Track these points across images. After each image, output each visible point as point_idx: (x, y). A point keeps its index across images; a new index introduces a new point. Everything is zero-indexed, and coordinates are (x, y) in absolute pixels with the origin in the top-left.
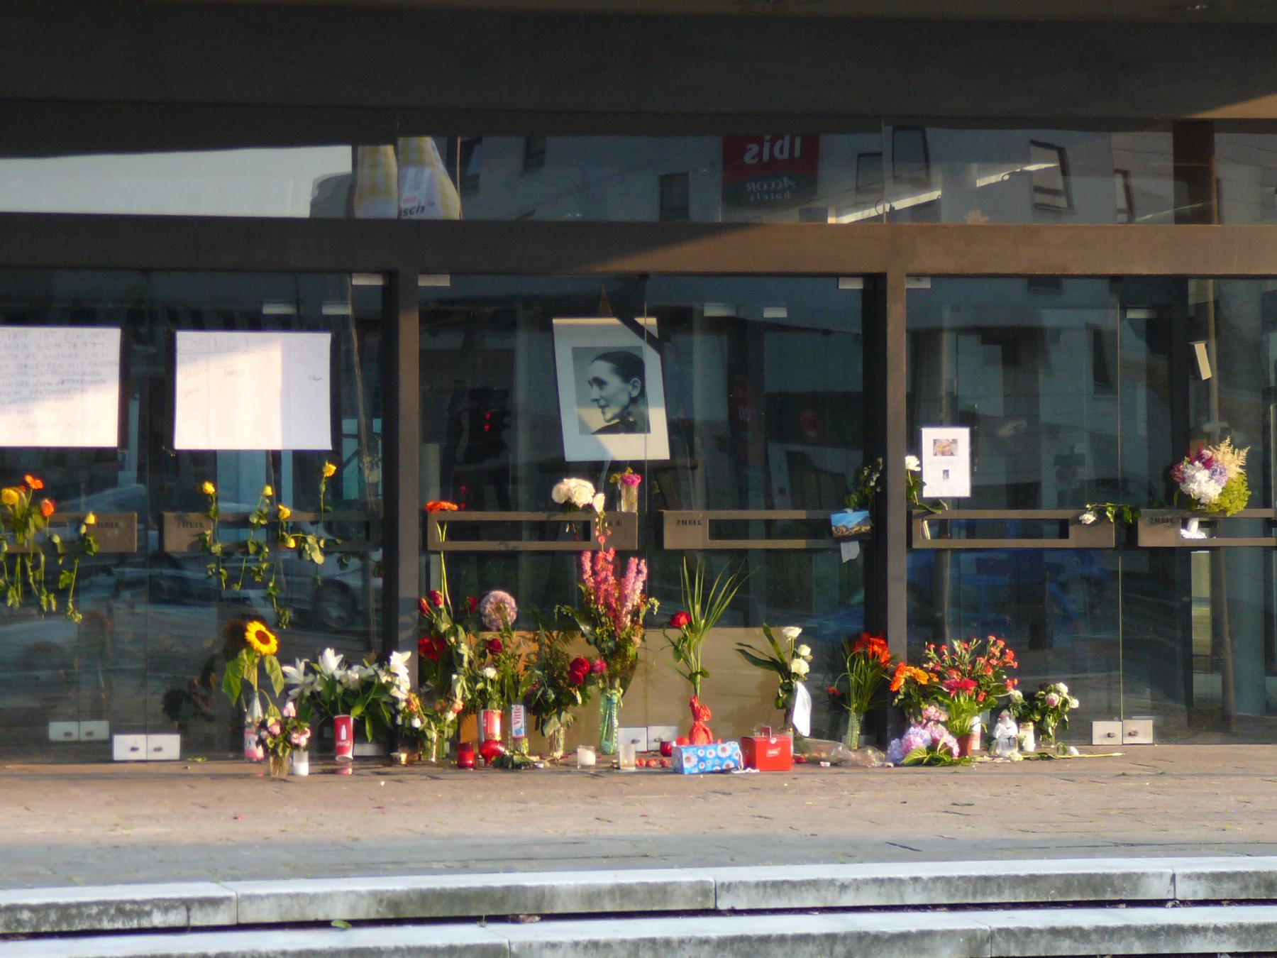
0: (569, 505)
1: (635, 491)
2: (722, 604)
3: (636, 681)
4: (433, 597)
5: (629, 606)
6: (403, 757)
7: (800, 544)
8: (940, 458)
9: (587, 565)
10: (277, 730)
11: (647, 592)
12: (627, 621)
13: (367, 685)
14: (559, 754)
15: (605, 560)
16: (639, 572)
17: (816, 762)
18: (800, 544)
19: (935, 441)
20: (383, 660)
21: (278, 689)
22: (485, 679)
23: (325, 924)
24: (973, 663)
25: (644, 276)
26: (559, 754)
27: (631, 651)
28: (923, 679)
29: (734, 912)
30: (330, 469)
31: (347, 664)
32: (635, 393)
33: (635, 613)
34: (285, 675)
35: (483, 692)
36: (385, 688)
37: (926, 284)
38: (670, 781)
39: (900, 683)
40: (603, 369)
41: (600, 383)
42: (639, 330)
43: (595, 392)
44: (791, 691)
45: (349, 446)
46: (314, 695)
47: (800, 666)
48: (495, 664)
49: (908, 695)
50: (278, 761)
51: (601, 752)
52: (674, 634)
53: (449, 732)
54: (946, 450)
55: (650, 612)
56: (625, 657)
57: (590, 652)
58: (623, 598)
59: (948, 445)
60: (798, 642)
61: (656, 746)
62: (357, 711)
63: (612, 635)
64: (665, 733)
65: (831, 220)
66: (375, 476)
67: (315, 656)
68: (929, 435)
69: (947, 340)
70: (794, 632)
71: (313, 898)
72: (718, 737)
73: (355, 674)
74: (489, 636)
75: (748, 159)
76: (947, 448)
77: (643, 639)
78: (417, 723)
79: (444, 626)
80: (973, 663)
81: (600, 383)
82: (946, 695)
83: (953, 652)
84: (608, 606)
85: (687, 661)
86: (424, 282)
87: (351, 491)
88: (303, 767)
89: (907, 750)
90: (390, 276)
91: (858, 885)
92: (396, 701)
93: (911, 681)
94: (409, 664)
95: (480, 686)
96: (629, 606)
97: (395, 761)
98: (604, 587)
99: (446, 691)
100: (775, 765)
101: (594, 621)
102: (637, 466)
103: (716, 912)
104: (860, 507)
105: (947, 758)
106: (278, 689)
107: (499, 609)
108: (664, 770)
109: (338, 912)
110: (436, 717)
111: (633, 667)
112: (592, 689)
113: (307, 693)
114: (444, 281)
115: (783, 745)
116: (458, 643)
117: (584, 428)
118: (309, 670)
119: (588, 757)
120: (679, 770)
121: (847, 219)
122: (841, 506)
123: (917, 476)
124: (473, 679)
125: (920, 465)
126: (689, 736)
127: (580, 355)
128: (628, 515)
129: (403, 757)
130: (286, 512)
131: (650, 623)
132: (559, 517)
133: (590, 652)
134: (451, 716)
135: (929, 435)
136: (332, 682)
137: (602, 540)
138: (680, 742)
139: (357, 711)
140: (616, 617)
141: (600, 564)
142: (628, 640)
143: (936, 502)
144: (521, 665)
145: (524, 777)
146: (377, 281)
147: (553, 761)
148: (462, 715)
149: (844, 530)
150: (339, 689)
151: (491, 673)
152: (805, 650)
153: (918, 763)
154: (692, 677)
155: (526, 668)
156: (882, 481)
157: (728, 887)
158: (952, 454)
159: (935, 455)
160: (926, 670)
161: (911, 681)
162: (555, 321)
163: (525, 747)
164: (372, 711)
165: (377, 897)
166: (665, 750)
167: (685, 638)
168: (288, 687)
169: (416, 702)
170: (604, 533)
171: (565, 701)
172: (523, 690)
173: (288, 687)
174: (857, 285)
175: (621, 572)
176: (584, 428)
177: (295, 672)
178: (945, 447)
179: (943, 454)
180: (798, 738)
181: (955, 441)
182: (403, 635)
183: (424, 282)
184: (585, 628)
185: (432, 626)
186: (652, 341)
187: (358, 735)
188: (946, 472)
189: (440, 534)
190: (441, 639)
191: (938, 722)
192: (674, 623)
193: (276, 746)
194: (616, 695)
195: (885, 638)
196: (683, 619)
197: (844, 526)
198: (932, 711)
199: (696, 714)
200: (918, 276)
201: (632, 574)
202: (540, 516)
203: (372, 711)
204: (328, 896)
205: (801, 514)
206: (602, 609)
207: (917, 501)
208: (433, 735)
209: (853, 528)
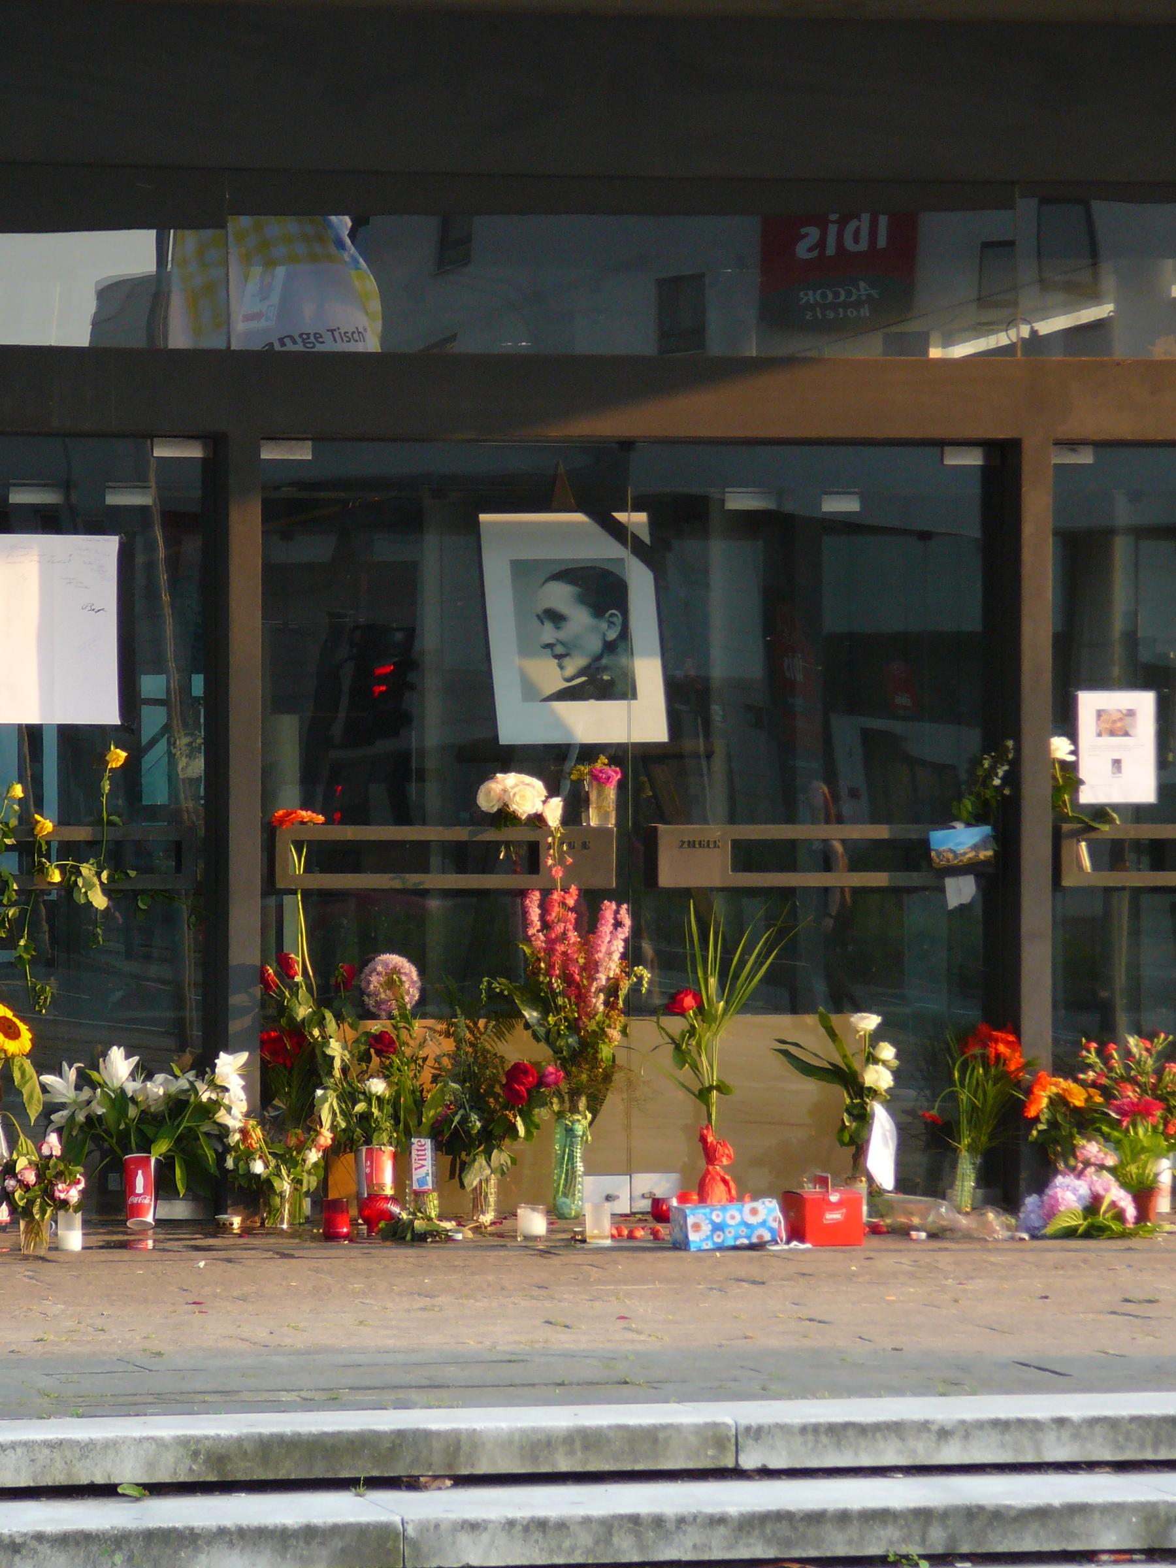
0: (505, 817)
1: (611, 793)
2: (751, 978)
3: (613, 1101)
4: (285, 966)
5: (602, 979)
6: (237, 1221)
7: (879, 879)
8: (1108, 740)
9: (535, 913)
10: (31, 1177)
11: (632, 956)
12: (599, 1002)
13: (178, 1105)
14: (487, 1218)
15: (563, 904)
16: (618, 924)
17: (903, 1232)
18: (879, 879)
19: (1100, 713)
20: (204, 1066)
21: (34, 1112)
22: (368, 1097)
23: (107, 1491)
24: (1159, 1072)
25: (627, 445)
26: (487, 1218)
27: (605, 1052)
28: (1078, 1098)
29: (766, 1473)
30: (118, 757)
31: (145, 1071)
32: (612, 635)
33: (612, 990)
34: (44, 1089)
35: (366, 1117)
36: (208, 1111)
37: (1086, 457)
38: (667, 1261)
39: (1041, 1104)
40: (560, 596)
41: (555, 617)
42: (619, 532)
43: (548, 633)
44: (863, 1118)
45: (152, 720)
46: (92, 1121)
47: (879, 1077)
48: (385, 1073)
49: (1053, 1124)
50: (34, 1228)
51: (555, 1214)
52: (675, 1024)
53: (311, 1182)
54: (1118, 727)
55: (636, 988)
56: (595, 1061)
57: (540, 1053)
58: (591, 967)
59: (1121, 719)
60: (877, 1036)
61: (645, 1205)
62: (161, 1148)
63: (574, 1026)
64: (661, 1184)
65: (935, 353)
66: (196, 767)
67: (94, 1059)
68: (1089, 703)
69: (1121, 548)
70: (870, 1022)
71: (86, 1448)
72: (745, 1191)
73: (158, 1087)
74: (375, 1027)
75: (802, 250)
76: (1119, 724)
77: (624, 1032)
78: (258, 1167)
79: (303, 1011)
80: (1159, 1072)
81: (555, 617)
82: (1115, 1125)
83: (1128, 1054)
84: (568, 979)
85: (695, 1068)
86: (270, 453)
87: (156, 791)
88: (74, 1238)
89: (1051, 1213)
90: (215, 442)
91: (968, 1430)
92: (224, 1131)
93: (1059, 1101)
94: (245, 1072)
95: (360, 1107)
96: (602, 979)
97: (223, 1229)
98: (560, 948)
99: (306, 1116)
100: (839, 1237)
101: (546, 1005)
102: (618, 754)
103: (737, 1473)
104: (975, 820)
105: (1115, 1226)
106: (34, 1112)
107: (392, 981)
108: (658, 1244)
109: (127, 1472)
110: (289, 1158)
111: (607, 1078)
112: (542, 1114)
113: (81, 1118)
114: (302, 452)
115: (850, 1205)
116: (326, 1038)
117: (530, 691)
118: (84, 1081)
119: (535, 1223)
120: (681, 1245)
121: (960, 351)
122: (945, 820)
123: (1070, 769)
124: (349, 1096)
125: (1074, 752)
126: (700, 1191)
127: (521, 570)
128: (601, 832)
129: (237, 1221)
130: (46, 826)
131: (636, 1006)
132: (490, 835)
133: (540, 1053)
134: (313, 1156)
135: (1089, 703)
136: (121, 1099)
137: (558, 873)
138: (683, 1198)
139: (161, 1148)
140: (581, 998)
141: (555, 912)
142: (601, 1034)
143: (1100, 813)
144: (427, 1074)
145: (430, 1254)
146: (194, 451)
147: (478, 1229)
148: (331, 1154)
149: (951, 856)
150: (132, 1112)
151: (378, 1086)
152: (887, 1052)
153: (1070, 1233)
154: (703, 1094)
155: (435, 1079)
156: (1013, 778)
157: (757, 1433)
158: (1126, 734)
159: (1099, 735)
160: (1083, 1084)
161: (1059, 1101)
162: (483, 517)
163: (433, 1206)
164: (186, 1145)
165: (191, 1447)
166: (659, 1212)
167: (692, 1031)
168: (50, 1109)
169: (257, 1134)
170: (561, 861)
171: (490, 1139)
172: (429, 1115)
173: (50, 1109)
174: (973, 459)
175: (588, 923)
176: (530, 691)
177: (62, 1084)
178: (1114, 722)
179: (1112, 733)
180: (875, 1192)
181: (1131, 713)
182: (236, 1026)
183: (270, 453)
184: (531, 1015)
185: (283, 1011)
186: (639, 549)
187: (163, 1187)
188: (1117, 763)
189: (296, 863)
190: (298, 1031)
191: (1102, 1167)
192: (674, 1007)
193: (31, 1203)
194: (581, 1124)
195: (1017, 1032)
196: (689, 1001)
197: (951, 850)
198: (1092, 1149)
199: (710, 1155)
200: (1072, 444)
201: (606, 928)
202: (460, 834)
203: (186, 1145)
204: (111, 1446)
205: (881, 832)
206: (557, 984)
207: (1069, 811)
208: (285, 1186)
209: (965, 854)
